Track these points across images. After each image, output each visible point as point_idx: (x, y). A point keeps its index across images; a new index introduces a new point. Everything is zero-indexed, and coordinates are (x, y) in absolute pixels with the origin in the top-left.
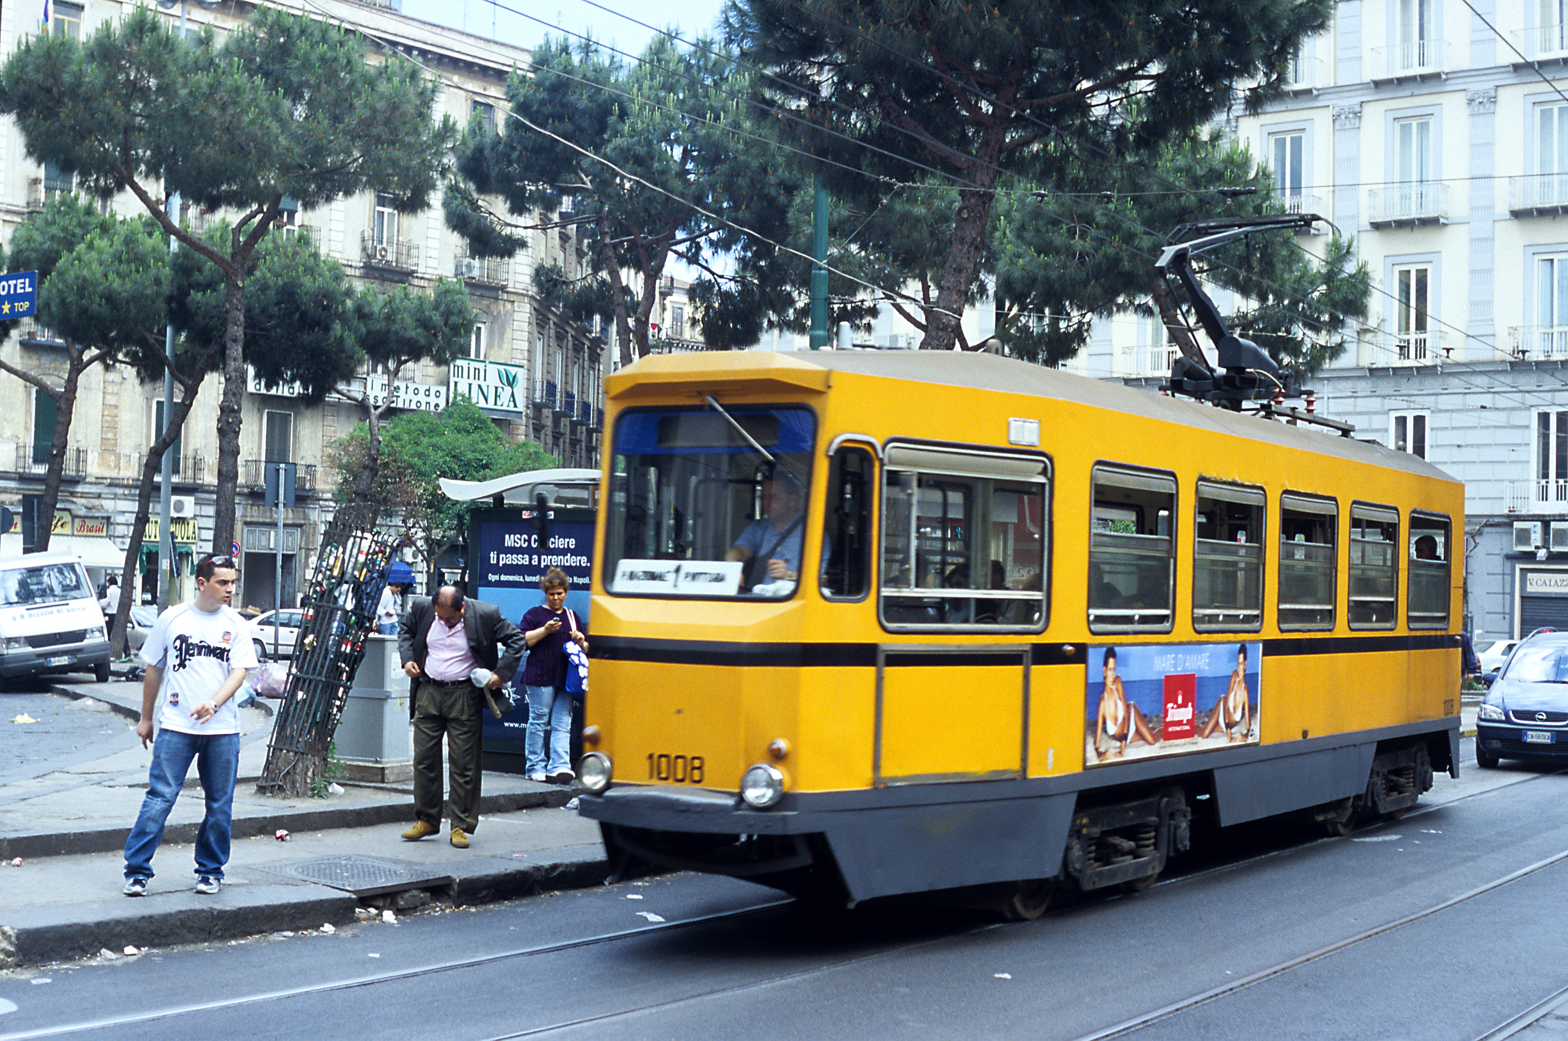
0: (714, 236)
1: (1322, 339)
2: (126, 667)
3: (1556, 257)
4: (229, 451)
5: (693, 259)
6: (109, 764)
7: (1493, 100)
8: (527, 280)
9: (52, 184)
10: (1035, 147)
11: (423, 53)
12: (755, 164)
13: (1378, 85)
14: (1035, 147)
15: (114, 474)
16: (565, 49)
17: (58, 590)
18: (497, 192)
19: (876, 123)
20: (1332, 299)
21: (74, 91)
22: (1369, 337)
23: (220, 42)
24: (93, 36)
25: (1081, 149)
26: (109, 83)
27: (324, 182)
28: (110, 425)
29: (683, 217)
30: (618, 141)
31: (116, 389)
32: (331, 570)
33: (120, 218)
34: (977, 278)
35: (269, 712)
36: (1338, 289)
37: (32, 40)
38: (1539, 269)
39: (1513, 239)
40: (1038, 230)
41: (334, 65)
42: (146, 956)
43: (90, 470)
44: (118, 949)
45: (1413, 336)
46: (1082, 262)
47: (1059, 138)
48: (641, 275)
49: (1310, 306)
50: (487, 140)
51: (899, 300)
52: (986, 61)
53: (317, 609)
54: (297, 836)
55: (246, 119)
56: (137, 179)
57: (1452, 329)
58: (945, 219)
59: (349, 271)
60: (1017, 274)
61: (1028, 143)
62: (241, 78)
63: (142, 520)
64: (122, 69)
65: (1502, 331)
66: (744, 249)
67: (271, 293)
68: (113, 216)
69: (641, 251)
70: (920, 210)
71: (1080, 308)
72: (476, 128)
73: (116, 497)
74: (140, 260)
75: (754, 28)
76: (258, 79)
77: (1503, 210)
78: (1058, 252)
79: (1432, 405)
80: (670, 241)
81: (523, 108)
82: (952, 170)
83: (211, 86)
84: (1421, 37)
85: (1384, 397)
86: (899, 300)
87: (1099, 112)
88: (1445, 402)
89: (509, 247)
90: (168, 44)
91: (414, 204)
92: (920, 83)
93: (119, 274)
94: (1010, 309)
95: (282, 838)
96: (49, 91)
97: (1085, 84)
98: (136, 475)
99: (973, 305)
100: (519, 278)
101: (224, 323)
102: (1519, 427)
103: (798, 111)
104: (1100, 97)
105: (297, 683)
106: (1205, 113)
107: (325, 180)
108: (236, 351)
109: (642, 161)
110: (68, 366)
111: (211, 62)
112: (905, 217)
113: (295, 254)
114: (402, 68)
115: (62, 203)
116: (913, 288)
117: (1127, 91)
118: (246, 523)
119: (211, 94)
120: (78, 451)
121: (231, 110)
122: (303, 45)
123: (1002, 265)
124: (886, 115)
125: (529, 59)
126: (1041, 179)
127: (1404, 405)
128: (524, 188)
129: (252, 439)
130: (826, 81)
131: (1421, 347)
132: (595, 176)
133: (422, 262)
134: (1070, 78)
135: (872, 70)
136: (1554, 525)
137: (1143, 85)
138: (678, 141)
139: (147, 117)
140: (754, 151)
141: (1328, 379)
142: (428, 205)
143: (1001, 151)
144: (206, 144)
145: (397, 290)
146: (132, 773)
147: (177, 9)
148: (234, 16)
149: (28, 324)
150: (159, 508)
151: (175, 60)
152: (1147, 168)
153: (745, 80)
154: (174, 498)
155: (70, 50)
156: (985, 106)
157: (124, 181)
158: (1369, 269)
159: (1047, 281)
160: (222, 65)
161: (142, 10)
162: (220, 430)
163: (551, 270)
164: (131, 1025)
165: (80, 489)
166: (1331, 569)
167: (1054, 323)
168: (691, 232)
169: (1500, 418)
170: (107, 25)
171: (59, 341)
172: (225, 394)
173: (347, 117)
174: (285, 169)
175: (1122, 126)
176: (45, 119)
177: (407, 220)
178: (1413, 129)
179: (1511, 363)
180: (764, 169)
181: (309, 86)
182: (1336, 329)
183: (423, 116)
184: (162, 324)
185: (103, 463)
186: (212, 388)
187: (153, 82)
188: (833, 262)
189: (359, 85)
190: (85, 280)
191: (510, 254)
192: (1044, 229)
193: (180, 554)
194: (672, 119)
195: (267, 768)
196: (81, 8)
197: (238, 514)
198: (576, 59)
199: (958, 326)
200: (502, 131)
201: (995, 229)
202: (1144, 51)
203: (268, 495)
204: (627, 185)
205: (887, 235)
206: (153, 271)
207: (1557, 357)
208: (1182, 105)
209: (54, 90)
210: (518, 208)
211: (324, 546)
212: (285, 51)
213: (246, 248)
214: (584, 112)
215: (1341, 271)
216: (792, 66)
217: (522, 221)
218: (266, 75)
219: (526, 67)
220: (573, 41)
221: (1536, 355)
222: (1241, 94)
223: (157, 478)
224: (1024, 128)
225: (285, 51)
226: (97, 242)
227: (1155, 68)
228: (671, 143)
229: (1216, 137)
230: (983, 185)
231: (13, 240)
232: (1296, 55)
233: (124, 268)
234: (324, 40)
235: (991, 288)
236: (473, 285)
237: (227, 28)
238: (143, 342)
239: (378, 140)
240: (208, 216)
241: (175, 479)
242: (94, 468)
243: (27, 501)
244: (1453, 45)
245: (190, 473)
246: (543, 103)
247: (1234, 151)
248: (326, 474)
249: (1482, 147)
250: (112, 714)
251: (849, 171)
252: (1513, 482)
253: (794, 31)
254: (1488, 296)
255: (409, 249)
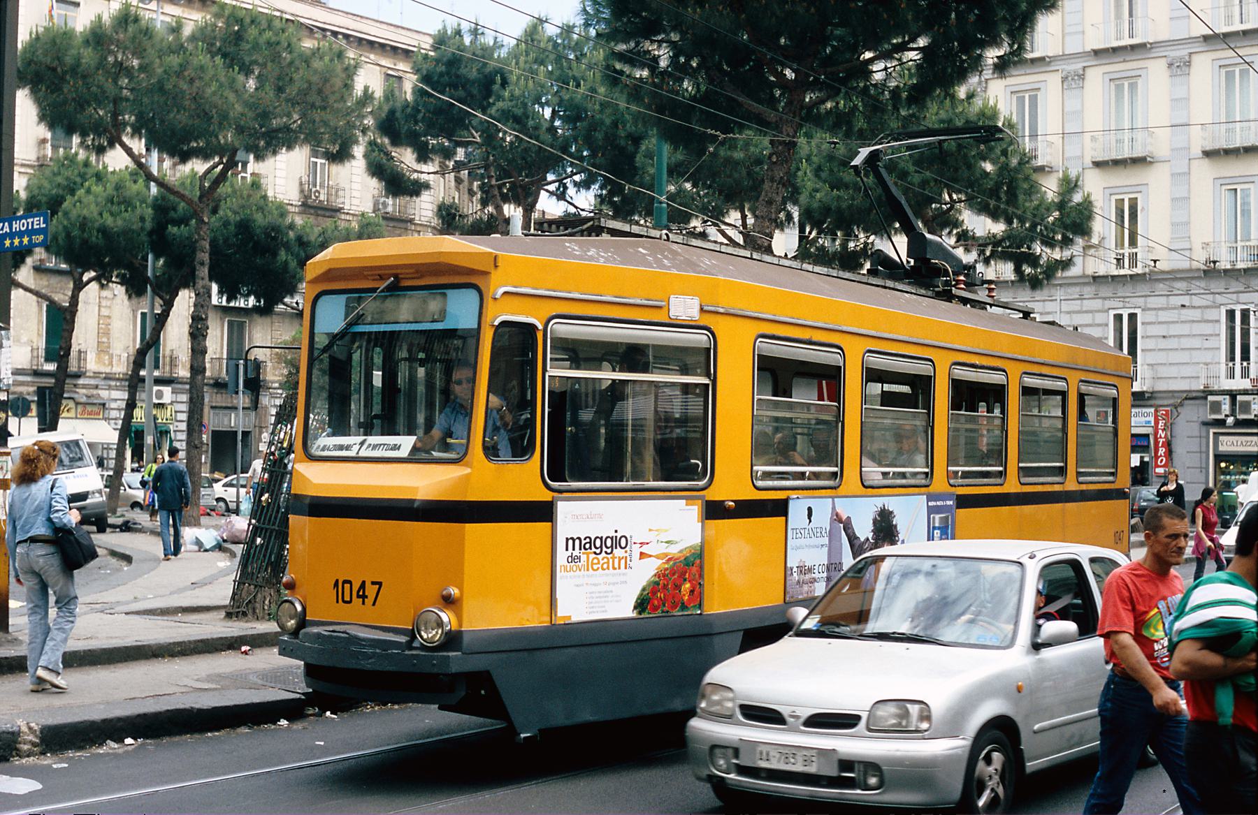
0: (577, 178)
1: (1057, 254)
2: (119, 521)
3: (1239, 187)
4: (198, 351)
5: (561, 196)
6: (109, 596)
7: (1188, 64)
8: (430, 214)
9: (57, 143)
10: (829, 105)
11: (346, 36)
12: (608, 121)
13: (1096, 53)
14: (829, 105)
15: (108, 370)
16: (458, 33)
17: (66, 461)
18: (409, 144)
19: (703, 88)
20: (1063, 223)
21: (74, 70)
22: (1092, 251)
23: (187, 31)
24: (88, 26)
25: (865, 106)
26: (101, 64)
27: (270, 140)
28: (104, 331)
29: (553, 163)
30: (500, 104)
31: (108, 303)
32: (282, 443)
33: (110, 169)
34: (784, 209)
35: (233, 555)
36: (1068, 214)
37: (41, 30)
38: (1226, 198)
39: (1205, 172)
40: (831, 171)
41: (278, 48)
42: (142, 744)
43: (89, 366)
44: (120, 740)
45: (1127, 251)
46: (866, 195)
47: (848, 97)
48: (520, 209)
49: (1046, 228)
50: (399, 105)
51: (723, 227)
52: (790, 38)
53: (271, 473)
54: (257, 651)
55: (209, 91)
56: (125, 139)
57: (1158, 242)
58: (759, 162)
59: (292, 209)
60: (815, 205)
61: (823, 102)
62: (204, 59)
63: (131, 405)
64: (111, 52)
65: (1197, 246)
66: (601, 188)
67: (232, 228)
68: (105, 167)
69: (519, 190)
70: (738, 155)
71: (865, 231)
72: (389, 95)
73: (110, 388)
74: (127, 203)
75: (606, 13)
76: (218, 59)
77: (1197, 151)
78: (847, 187)
79: (1142, 304)
80: (542, 183)
81: (426, 79)
82: (763, 124)
83: (181, 65)
84: (1131, 15)
85: (1105, 298)
86: (723, 227)
87: (878, 77)
88: (1154, 302)
89: (416, 189)
90: (148, 32)
91: (341, 155)
92: (738, 55)
93: (112, 214)
94: (810, 233)
95: (246, 653)
96: (54, 70)
97: (868, 55)
98: (124, 370)
99: (782, 230)
100: (424, 213)
101: (194, 251)
102: (1211, 321)
103: (641, 79)
104: (878, 66)
105: (256, 531)
106: (962, 75)
107: (272, 138)
108: (204, 272)
109: (519, 120)
110: (71, 285)
111: (182, 46)
112: (729, 161)
113: (249, 196)
114: (331, 49)
115: (66, 158)
116: (734, 217)
117: (900, 60)
118: (212, 407)
119: (182, 72)
120: (80, 352)
121: (197, 83)
122: (252, 32)
123: (803, 198)
124: (711, 80)
125: (431, 41)
126: (833, 129)
127: (1121, 304)
128: (427, 143)
129: (217, 342)
130: (664, 57)
131: (1134, 259)
132: (483, 132)
133: (347, 201)
134: (856, 50)
135: (699, 44)
136: (1239, 398)
137: (913, 55)
138: (547, 103)
139: (132, 90)
140: (609, 111)
141: (1060, 285)
142: (353, 157)
143: (802, 108)
144: (178, 111)
145: (328, 223)
146: (127, 603)
147: (153, 6)
148: (199, 10)
149: (40, 253)
150: (144, 396)
151: (153, 46)
152: (918, 119)
153: (600, 55)
154: (156, 388)
155: (70, 38)
156: (790, 74)
157: (114, 140)
158: (1093, 198)
159: (839, 210)
160: (190, 48)
161: (127, 6)
162: (191, 334)
163: (451, 206)
164: (130, 799)
165: (81, 381)
166: (837, 423)
167: (844, 245)
168: (560, 175)
169: (1196, 314)
170: (99, 17)
171: (64, 266)
172: (195, 305)
173: (293, 91)
174: (240, 130)
175: (897, 87)
176: (52, 92)
177: (336, 169)
178: (1125, 87)
179: (1205, 271)
180: (615, 124)
181: (258, 64)
182: (1067, 245)
183: (348, 86)
184: (146, 252)
185: (99, 360)
186: (184, 301)
187: (136, 63)
188: (671, 197)
189: (297, 62)
190: (85, 218)
191: (418, 194)
192: (836, 170)
193: (161, 432)
194: (543, 86)
195: (233, 598)
196: (78, 5)
197: (206, 400)
198: (467, 40)
199: (770, 246)
200: (409, 97)
201: (799, 169)
202: (914, 28)
203: (231, 386)
204: (508, 139)
205: (714, 175)
206: (138, 211)
207: (1240, 265)
208: (944, 70)
209: (59, 70)
210: (423, 157)
211: (275, 425)
212: (239, 37)
213: (210, 191)
214: (474, 82)
215: (1070, 201)
216: (637, 44)
217: (424, 168)
218: (225, 56)
219: (428, 47)
220: (465, 26)
221: (1224, 265)
222: (990, 61)
223: (142, 373)
224: (820, 90)
225: (239, 37)
226: (94, 188)
227: (922, 42)
228: (542, 105)
229: (971, 96)
230: (788, 135)
231: (27, 188)
232: (1033, 30)
233: (115, 208)
234: (270, 27)
235: (796, 216)
236: (388, 218)
237: (193, 19)
238: (129, 266)
239: (313, 106)
240: (180, 167)
241: (156, 373)
242: (92, 365)
243: (41, 392)
244: (1156, 21)
245: (167, 368)
246: (441, 75)
247: (985, 106)
248: (274, 368)
249: (1180, 102)
250: (109, 558)
251: (685, 125)
252: (1207, 364)
253: (638, 15)
254: (1184, 218)
255: (337, 191)
